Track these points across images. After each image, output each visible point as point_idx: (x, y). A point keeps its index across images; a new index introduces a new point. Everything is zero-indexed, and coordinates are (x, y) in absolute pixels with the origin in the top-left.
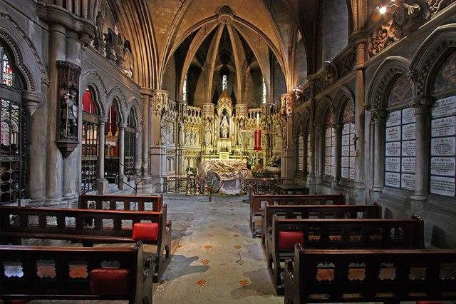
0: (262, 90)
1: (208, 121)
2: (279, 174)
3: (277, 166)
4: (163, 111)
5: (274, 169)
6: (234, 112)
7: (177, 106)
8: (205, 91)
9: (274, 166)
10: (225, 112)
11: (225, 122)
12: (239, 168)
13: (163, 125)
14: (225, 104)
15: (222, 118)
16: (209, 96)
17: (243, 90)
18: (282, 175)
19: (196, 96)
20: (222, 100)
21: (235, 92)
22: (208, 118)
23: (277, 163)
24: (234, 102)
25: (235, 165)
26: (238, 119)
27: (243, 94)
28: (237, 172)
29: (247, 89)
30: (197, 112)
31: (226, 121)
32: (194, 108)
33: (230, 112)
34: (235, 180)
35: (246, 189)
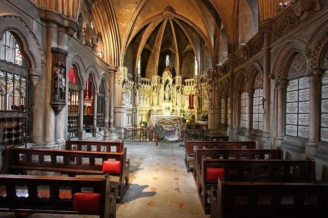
0: (194, 66)
2: (207, 126)
13: (123, 91)
29: (183, 65)
30: (148, 82)
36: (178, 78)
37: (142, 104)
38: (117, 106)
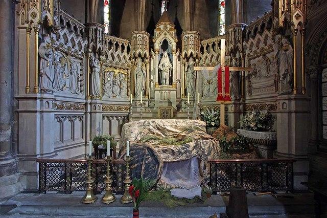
0: (219, 15)
1: (139, 60)
2: (272, 145)
3: (265, 130)
4: (45, 24)
5: (261, 135)
6: (179, 45)
7: (87, 31)
8: (136, 17)
9: (259, 130)
10: (165, 45)
11: (166, 60)
12: (194, 135)
13: (43, 52)
14: (165, 32)
15: (162, 55)
16: (142, 22)
17: (192, 14)
18: (282, 148)
19: (123, 25)
20: (162, 27)
21: (179, 18)
22: (140, 55)
23: (266, 123)
24: (179, 32)
25: (185, 129)
26: (186, 55)
27: (192, 20)
28: (192, 144)
29: (197, 12)
30: (123, 47)
31: (168, 59)
32: (118, 39)
33: (173, 45)
34: (188, 161)
35: (212, 181)
36: (190, 37)
37: (111, 94)
38: (22, 94)
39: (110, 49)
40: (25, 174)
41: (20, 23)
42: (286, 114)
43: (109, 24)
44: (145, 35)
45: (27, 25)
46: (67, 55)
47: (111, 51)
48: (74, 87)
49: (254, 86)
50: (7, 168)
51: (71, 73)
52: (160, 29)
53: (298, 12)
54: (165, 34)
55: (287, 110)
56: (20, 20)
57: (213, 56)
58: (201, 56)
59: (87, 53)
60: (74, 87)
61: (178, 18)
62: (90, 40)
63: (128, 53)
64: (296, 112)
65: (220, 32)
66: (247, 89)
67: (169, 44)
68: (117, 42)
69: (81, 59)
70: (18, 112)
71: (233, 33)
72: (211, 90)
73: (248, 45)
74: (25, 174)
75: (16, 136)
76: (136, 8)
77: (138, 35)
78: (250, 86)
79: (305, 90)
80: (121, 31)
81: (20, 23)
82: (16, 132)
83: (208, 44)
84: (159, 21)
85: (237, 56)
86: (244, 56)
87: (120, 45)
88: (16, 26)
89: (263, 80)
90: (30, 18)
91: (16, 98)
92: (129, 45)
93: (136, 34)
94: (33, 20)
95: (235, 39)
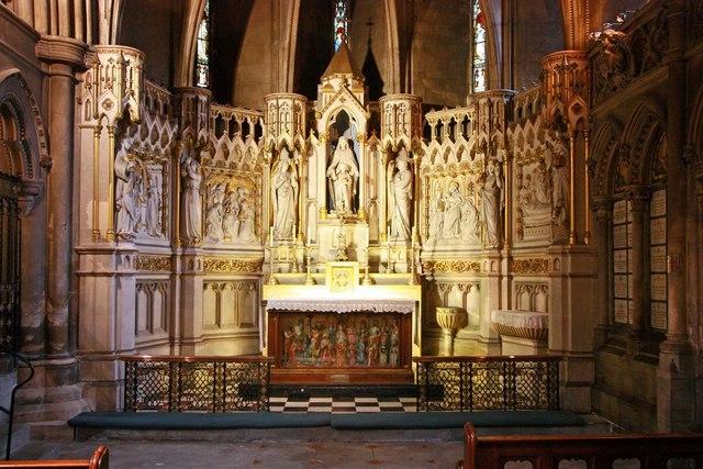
4: (124, 121)
6: (374, 126)
8: (275, 55)
10: (342, 123)
11: (342, 156)
14: (338, 93)
16: (286, 68)
24: (374, 92)
29: (417, 43)
30: (246, 126)
39: (219, 135)
40: (94, 384)
41: (83, 117)
42: (559, 280)
43: (209, 65)
44: (296, 102)
45: (95, 122)
46: (143, 160)
47: (220, 141)
48: (154, 223)
49: (527, 221)
50: (68, 372)
51: (149, 195)
52: (328, 86)
53: (577, 101)
54: (343, 100)
55: (561, 272)
56: (82, 111)
57: (448, 150)
58: (424, 146)
59: (174, 152)
60: (154, 223)
61: (374, 51)
62: (183, 122)
63: (257, 140)
64: (572, 276)
65: (475, 84)
66: (516, 226)
67: (351, 120)
68: (233, 118)
69: (164, 163)
70: (79, 275)
71: (487, 108)
72: (447, 225)
73: (516, 137)
74: (94, 384)
75: (74, 317)
76: (275, 36)
77: (281, 102)
78: (520, 220)
79: (589, 237)
80: (237, 83)
81: (83, 117)
82: (74, 312)
83: (440, 121)
84: (329, 68)
85: (499, 157)
86: (510, 157)
87: (240, 122)
88: (76, 125)
89: (539, 212)
90: (101, 110)
91: (77, 251)
92: (259, 122)
93: (277, 99)
94: (106, 112)
95: (491, 122)
